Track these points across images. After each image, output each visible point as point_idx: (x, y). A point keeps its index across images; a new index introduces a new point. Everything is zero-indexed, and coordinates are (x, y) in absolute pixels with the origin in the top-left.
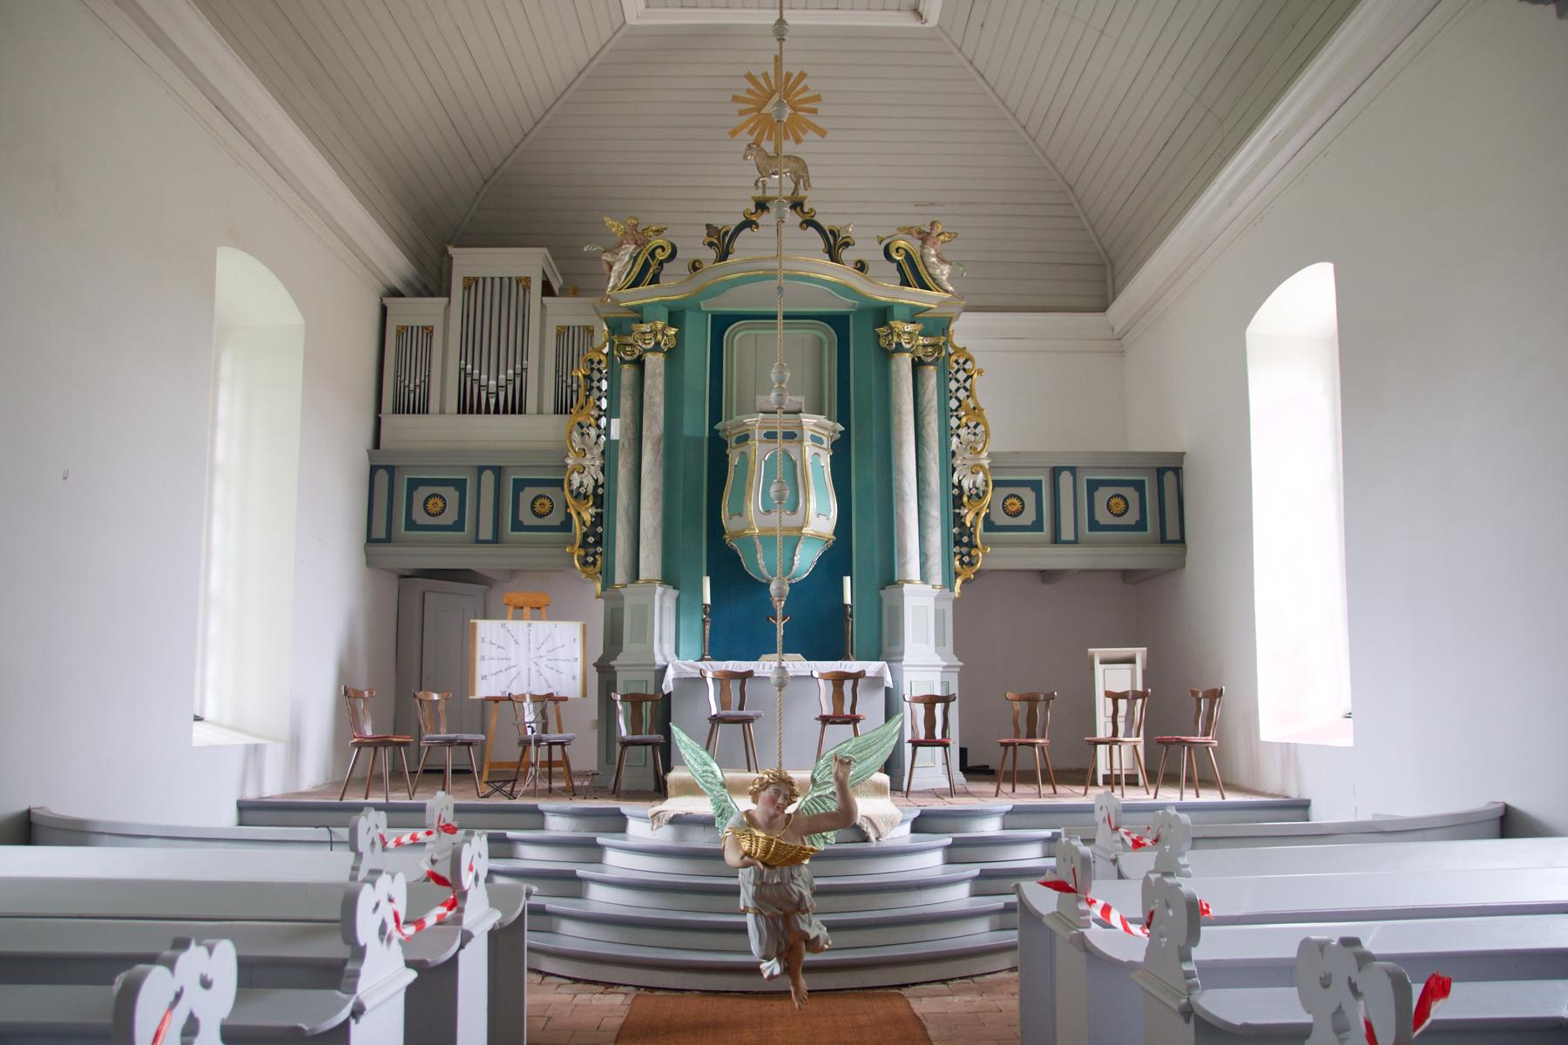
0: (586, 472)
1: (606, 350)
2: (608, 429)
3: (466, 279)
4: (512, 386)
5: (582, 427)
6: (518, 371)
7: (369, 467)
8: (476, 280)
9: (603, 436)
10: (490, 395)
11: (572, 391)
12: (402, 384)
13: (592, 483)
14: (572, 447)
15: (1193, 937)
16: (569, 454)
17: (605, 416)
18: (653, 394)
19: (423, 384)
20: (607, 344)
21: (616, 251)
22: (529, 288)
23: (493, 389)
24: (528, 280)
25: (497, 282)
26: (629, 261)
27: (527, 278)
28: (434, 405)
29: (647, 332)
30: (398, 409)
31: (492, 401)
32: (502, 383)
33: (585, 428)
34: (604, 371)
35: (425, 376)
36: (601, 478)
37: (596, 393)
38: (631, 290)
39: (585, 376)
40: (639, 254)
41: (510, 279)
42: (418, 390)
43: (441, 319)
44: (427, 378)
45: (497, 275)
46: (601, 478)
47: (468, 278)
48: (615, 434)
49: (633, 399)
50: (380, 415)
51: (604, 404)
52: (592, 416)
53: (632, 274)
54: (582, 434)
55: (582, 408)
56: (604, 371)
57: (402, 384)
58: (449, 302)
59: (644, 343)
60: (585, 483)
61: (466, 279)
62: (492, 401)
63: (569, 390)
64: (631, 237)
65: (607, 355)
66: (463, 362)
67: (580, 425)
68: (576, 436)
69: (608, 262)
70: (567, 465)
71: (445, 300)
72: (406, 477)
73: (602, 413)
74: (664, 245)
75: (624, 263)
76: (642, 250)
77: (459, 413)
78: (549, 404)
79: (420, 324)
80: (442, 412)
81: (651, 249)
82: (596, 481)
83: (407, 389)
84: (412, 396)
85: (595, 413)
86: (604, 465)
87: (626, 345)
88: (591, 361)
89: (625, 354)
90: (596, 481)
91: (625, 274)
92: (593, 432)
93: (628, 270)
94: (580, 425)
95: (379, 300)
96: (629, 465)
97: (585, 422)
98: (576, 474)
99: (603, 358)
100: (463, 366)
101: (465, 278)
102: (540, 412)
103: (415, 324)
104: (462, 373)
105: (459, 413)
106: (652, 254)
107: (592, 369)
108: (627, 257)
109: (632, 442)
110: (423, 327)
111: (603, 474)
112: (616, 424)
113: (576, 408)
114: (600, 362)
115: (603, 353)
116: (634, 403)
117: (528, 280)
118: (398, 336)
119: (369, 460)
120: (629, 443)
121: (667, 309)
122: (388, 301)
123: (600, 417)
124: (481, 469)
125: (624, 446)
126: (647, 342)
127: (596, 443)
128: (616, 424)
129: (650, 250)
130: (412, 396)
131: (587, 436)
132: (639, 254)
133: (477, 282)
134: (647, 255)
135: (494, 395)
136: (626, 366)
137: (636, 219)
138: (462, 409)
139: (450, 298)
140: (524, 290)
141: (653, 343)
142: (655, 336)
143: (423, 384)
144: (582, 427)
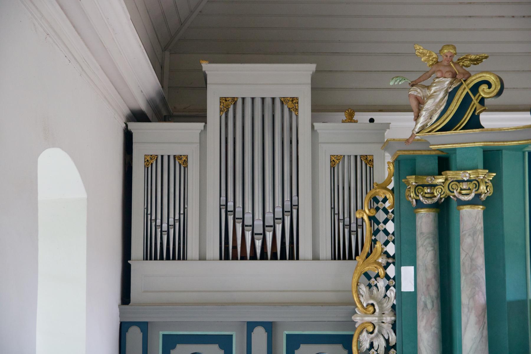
0: (376, 331)
1: (390, 187)
2: (397, 279)
3: (224, 100)
4: (281, 225)
5: (369, 277)
6: (287, 207)
7: (119, 323)
8: (234, 100)
9: (392, 288)
10: (256, 237)
11: (350, 232)
12: (154, 224)
13: (383, 344)
14: (360, 302)
15: (268, 231)
16: (356, 310)
17: (394, 263)
18: (475, 256)
19: (177, 224)
20: (393, 178)
21: (426, 83)
22: (297, 110)
23: (259, 229)
24: (294, 100)
25: (258, 104)
26: (444, 97)
27: (293, 99)
28: (192, 250)
29: (463, 181)
30: (149, 256)
31: (258, 244)
32: (269, 221)
33: (373, 279)
34: (390, 211)
35: (180, 214)
36: (393, 339)
37: (381, 237)
38: (444, 133)
39: (370, 218)
40: (456, 89)
41: (273, 99)
42: (172, 231)
43: (196, 147)
44: (182, 216)
45: (258, 95)
46: (393, 339)
47: (226, 99)
48: (407, 286)
49: (434, 250)
50: (129, 262)
51: (391, 249)
52: (380, 264)
53: (448, 112)
54: (370, 286)
55: (368, 255)
56: (390, 211)
57: (154, 224)
58: (205, 127)
59: (460, 193)
60: (375, 344)
61: (224, 100)
62: (258, 244)
63: (347, 231)
64: (448, 69)
65: (392, 191)
66: (223, 198)
67: (367, 275)
68: (364, 289)
69: (417, 98)
70: (355, 323)
71: (201, 125)
72: (161, 333)
73: (390, 260)
74: (491, 81)
75: (438, 100)
76: (462, 84)
77: (221, 259)
78: (326, 250)
79: (172, 154)
80: (202, 258)
81: (476, 82)
82: (387, 341)
83: (159, 230)
84: (165, 238)
85: (382, 260)
86: (395, 321)
87: (423, 186)
88: (376, 200)
89: (423, 197)
90: (387, 341)
91: (439, 111)
92: (382, 283)
93: (442, 108)
94: (367, 275)
95: (124, 125)
96: (433, 329)
97: (372, 270)
98: (365, 333)
99: (389, 196)
100: (224, 203)
101: (221, 98)
102: (316, 258)
103: (166, 154)
104: (223, 211)
105: (221, 259)
106: (475, 89)
107: (377, 209)
108: (441, 95)
109: (435, 301)
110: (175, 157)
111: (395, 332)
112: (408, 272)
113: (363, 255)
114: (385, 200)
115: (388, 190)
116: (435, 254)
117: (294, 100)
118: (146, 167)
119: (120, 316)
120: (433, 302)
121: (482, 150)
122: (133, 126)
123: (388, 264)
124: (251, 326)
125: (426, 305)
126: (463, 192)
127: (386, 296)
128: (408, 272)
129: (471, 85)
130: (165, 238)
131: (375, 288)
132: (456, 89)
133: (235, 104)
134: (467, 90)
135: (232, 213)
136: (423, 211)
137: (455, 48)
138: (225, 256)
139: (206, 123)
140: (290, 112)
141: (473, 195)
142: (478, 186)
143: (177, 224)
144: (369, 277)
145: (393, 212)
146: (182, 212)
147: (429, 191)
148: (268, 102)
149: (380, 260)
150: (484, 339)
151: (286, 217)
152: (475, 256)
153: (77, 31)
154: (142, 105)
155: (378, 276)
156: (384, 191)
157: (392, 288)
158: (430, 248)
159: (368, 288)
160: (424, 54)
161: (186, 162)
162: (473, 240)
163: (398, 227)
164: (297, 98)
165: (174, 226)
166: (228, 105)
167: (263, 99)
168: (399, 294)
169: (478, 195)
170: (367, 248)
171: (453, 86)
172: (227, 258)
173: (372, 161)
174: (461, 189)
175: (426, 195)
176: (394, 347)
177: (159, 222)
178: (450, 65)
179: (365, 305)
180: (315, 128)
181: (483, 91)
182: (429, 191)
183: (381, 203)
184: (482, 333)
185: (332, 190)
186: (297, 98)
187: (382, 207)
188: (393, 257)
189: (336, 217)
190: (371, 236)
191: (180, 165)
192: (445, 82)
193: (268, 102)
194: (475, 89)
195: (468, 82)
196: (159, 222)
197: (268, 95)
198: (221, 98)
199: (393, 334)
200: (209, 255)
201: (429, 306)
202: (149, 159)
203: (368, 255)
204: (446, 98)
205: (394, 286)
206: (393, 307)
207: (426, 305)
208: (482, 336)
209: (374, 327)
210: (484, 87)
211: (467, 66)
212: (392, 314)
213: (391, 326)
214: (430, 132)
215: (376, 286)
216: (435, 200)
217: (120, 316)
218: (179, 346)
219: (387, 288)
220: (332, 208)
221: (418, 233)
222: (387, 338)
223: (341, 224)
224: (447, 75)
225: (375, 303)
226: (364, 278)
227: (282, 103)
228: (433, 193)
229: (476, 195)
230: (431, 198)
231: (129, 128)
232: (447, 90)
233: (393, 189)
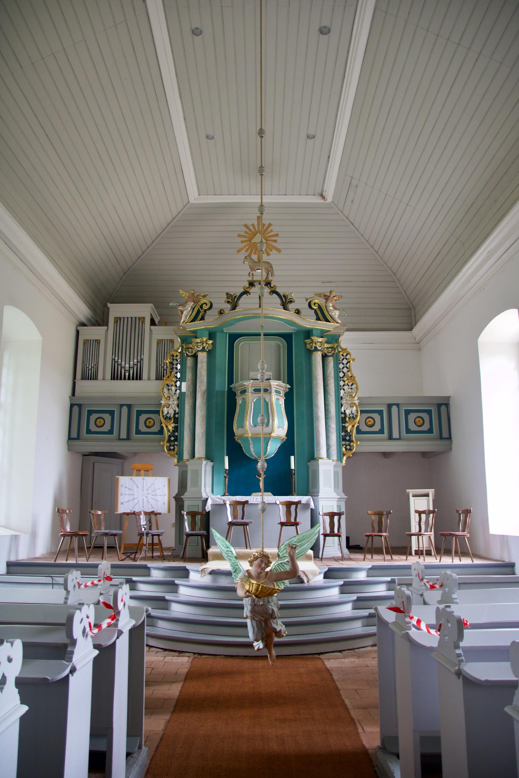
1: (179, 351)
2: (180, 387)
8: (120, 318)
9: (178, 390)
11: (164, 369)
16: (162, 398)
17: (179, 381)
18: (202, 371)
19: (95, 366)
20: (180, 348)
22: (144, 322)
24: (144, 318)
28: (100, 376)
30: (83, 378)
31: (127, 374)
33: (170, 387)
34: (179, 360)
35: (96, 362)
39: (170, 363)
40: (195, 307)
41: (136, 318)
42: (93, 369)
43: (104, 336)
44: (97, 363)
48: (184, 389)
49: (192, 373)
52: (173, 381)
53: (192, 315)
54: (169, 389)
55: (168, 377)
56: (179, 360)
58: (108, 329)
59: (197, 347)
60: (170, 412)
62: (127, 374)
63: (162, 369)
64: (192, 299)
67: (168, 385)
68: (166, 390)
69: (181, 310)
70: (161, 404)
71: (106, 328)
72: (87, 409)
73: (177, 380)
74: (207, 303)
78: (153, 375)
82: (175, 411)
84: (90, 372)
85: (174, 379)
86: (178, 403)
87: (189, 348)
88: (173, 356)
90: (175, 411)
91: (189, 315)
92: (174, 388)
93: (190, 314)
94: (168, 385)
98: (165, 408)
99: (178, 354)
100: (114, 358)
101: (115, 318)
109: (192, 393)
110: (95, 340)
111: (178, 408)
112: (184, 384)
113: (166, 377)
114: (177, 356)
115: (178, 352)
117: (144, 318)
118: (84, 344)
120: (190, 393)
122: (80, 328)
123: (177, 381)
124: (122, 406)
125: (188, 395)
127: (175, 393)
130: (90, 372)
131: (170, 390)
132: (195, 307)
134: (199, 307)
135: (128, 371)
136: (189, 358)
138: (113, 378)
141: (202, 347)
145: (180, 361)
146: (97, 362)
147: (191, 350)
148: (134, 319)
149: (173, 379)
150: (203, 403)
151: (138, 364)
152: (202, 371)
153: (33, 273)
154: (84, 320)
155: (172, 385)
156: (176, 352)
157: (178, 390)
158: (190, 373)
159: (168, 390)
160: (184, 294)
161: (99, 342)
162: (201, 365)
163: (182, 367)
164: (145, 317)
165: (94, 367)
166: (117, 320)
167: (132, 318)
168: (181, 393)
169: (204, 348)
170: (168, 374)
171: (194, 306)
172: (114, 379)
173: (173, 341)
174: (198, 346)
175: (190, 352)
176: (178, 413)
177: (88, 365)
178: (193, 298)
179: (166, 396)
180: (151, 328)
181: (204, 306)
182: (191, 350)
183: (175, 357)
184: (203, 401)
185: (157, 353)
186: (145, 317)
187: (175, 359)
188: (179, 378)
189: (158, 363)
190: (170, 370)
191: (97, 343)
192: (191, 304)
193: (134, 319)
194: (201, 307)
195: (199, 304)
196: (88, 365)
197: (133, 316)
198: (115, 318)
199: (178, 409)
200: (106, 378)
201: (189, 395)
202: (85, 341)
203: (168, 377)
204: (192, 310)
205: (179, 390)
206: (178, 398)
207: (188, 395)
208: (203, 402)
209: (169, 405)
210: (204, 305)
211: (200, 299)
212: (177, 400)
213: (177, 405)
214: (186, 323)
215: (171, 389)
216: (193, 353)
217: (70, 401)
218: (93, 414)
219: (176, 390)
220: (157, 360)
221: (187, 366)
222: (175, 410)
223: (160, 366)
224: (191, 301)
225: (170, 396)
226: (166, 386)
227: (139, 319)
228: (192, 351)
229: (203, 347)
230: (191, 353)
231: (78, 329)
232: (192, 307)
233: (180, 352)
